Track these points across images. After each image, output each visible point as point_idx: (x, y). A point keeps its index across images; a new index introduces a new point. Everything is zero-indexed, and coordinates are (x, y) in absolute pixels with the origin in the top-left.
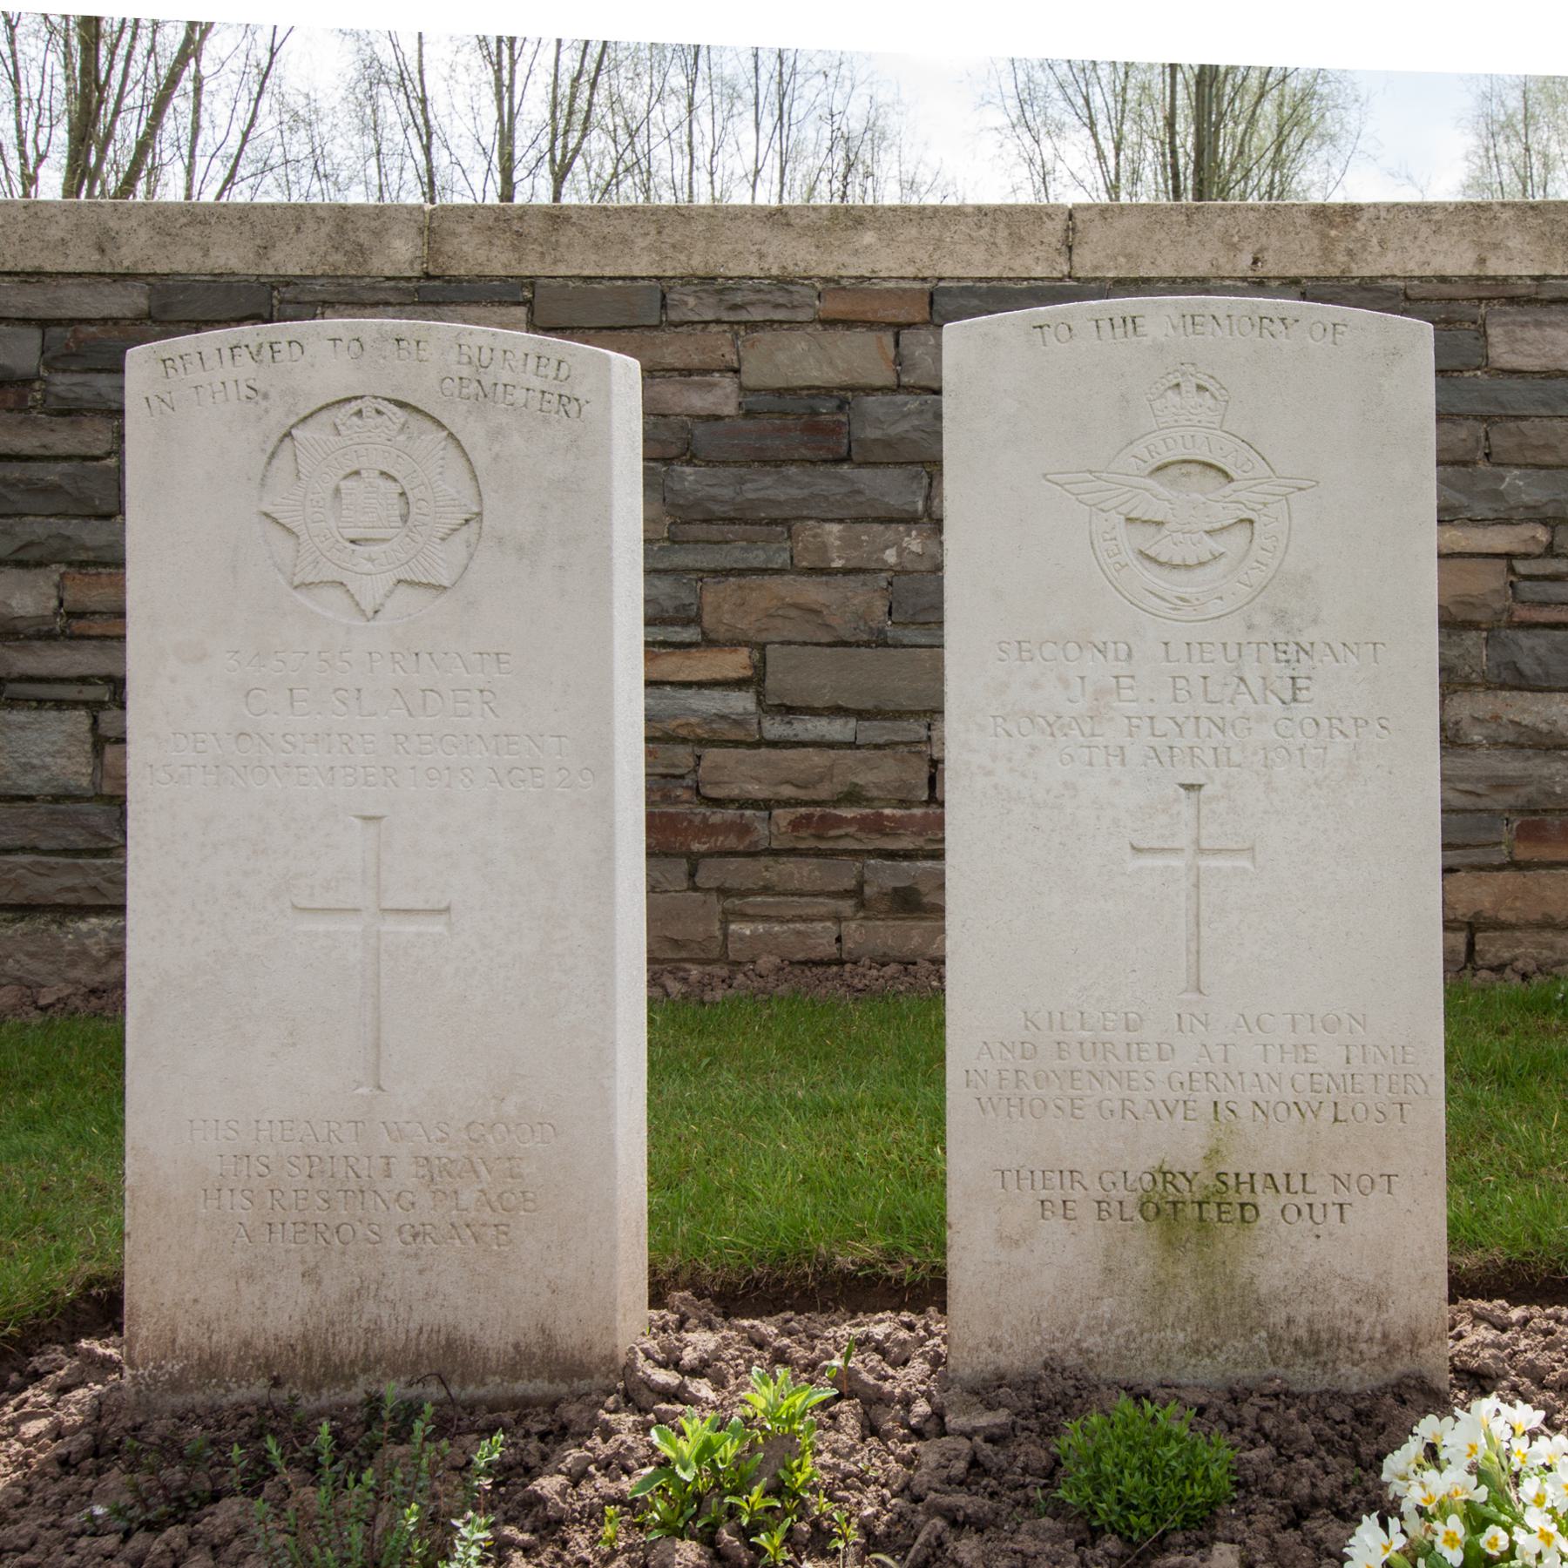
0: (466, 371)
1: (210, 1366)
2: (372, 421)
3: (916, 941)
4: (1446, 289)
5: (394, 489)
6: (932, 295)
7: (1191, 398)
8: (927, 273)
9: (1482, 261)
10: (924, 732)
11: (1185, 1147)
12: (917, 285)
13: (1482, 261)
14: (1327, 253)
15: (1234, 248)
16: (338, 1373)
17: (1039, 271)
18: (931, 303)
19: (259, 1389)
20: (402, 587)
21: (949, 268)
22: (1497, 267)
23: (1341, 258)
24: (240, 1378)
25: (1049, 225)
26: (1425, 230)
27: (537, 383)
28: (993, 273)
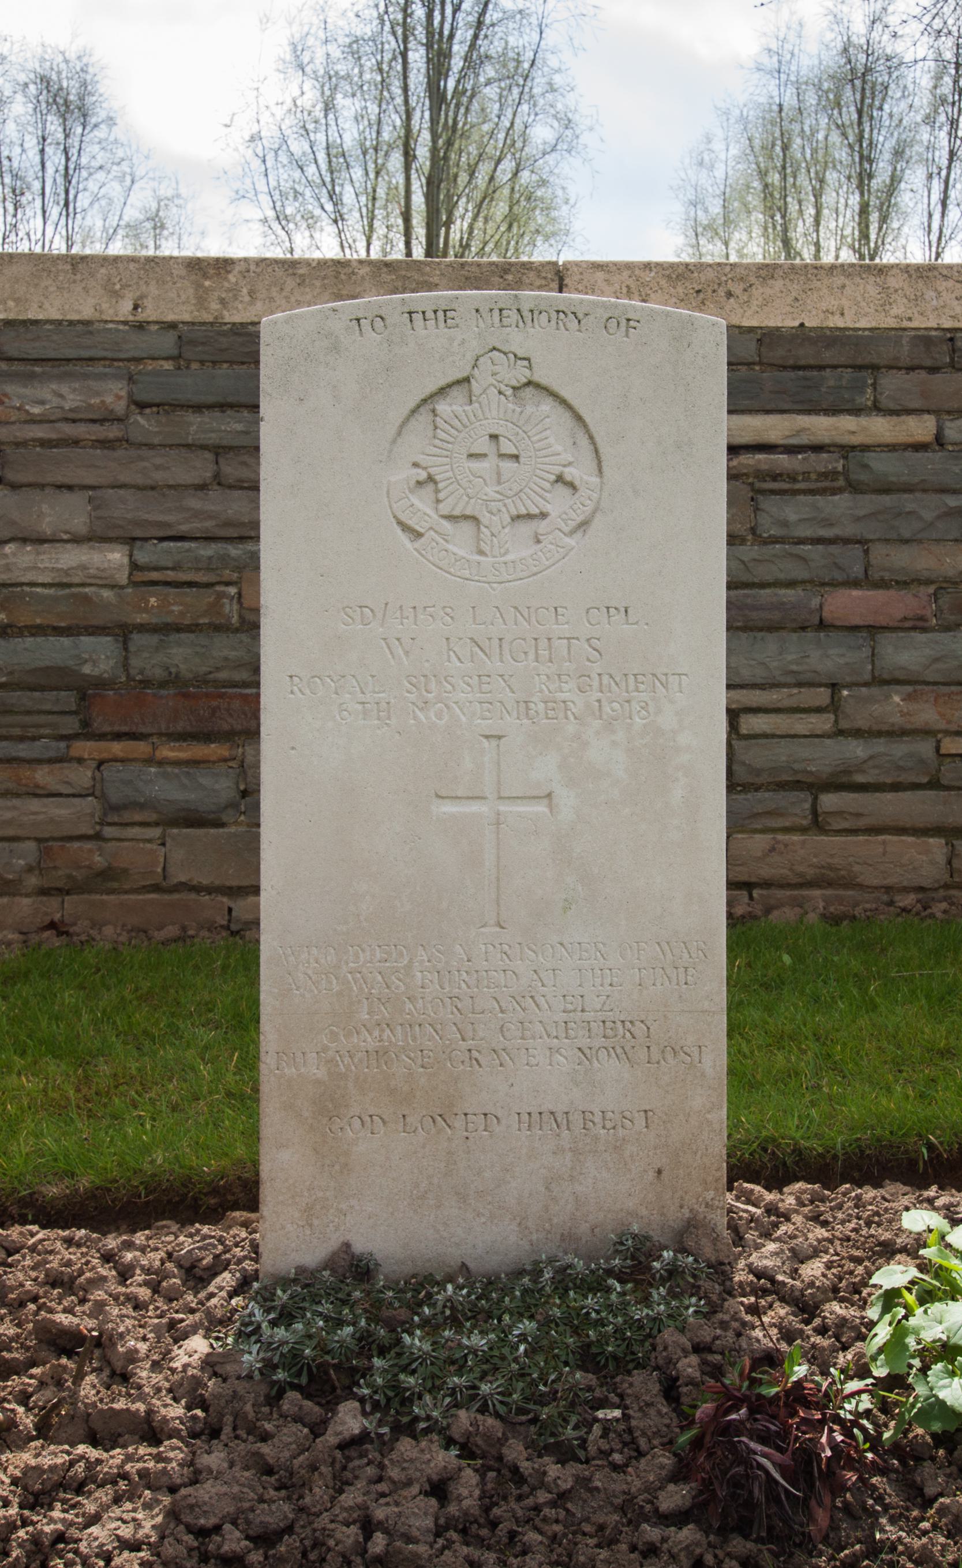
14: (201, 302)
23: (215, 306)
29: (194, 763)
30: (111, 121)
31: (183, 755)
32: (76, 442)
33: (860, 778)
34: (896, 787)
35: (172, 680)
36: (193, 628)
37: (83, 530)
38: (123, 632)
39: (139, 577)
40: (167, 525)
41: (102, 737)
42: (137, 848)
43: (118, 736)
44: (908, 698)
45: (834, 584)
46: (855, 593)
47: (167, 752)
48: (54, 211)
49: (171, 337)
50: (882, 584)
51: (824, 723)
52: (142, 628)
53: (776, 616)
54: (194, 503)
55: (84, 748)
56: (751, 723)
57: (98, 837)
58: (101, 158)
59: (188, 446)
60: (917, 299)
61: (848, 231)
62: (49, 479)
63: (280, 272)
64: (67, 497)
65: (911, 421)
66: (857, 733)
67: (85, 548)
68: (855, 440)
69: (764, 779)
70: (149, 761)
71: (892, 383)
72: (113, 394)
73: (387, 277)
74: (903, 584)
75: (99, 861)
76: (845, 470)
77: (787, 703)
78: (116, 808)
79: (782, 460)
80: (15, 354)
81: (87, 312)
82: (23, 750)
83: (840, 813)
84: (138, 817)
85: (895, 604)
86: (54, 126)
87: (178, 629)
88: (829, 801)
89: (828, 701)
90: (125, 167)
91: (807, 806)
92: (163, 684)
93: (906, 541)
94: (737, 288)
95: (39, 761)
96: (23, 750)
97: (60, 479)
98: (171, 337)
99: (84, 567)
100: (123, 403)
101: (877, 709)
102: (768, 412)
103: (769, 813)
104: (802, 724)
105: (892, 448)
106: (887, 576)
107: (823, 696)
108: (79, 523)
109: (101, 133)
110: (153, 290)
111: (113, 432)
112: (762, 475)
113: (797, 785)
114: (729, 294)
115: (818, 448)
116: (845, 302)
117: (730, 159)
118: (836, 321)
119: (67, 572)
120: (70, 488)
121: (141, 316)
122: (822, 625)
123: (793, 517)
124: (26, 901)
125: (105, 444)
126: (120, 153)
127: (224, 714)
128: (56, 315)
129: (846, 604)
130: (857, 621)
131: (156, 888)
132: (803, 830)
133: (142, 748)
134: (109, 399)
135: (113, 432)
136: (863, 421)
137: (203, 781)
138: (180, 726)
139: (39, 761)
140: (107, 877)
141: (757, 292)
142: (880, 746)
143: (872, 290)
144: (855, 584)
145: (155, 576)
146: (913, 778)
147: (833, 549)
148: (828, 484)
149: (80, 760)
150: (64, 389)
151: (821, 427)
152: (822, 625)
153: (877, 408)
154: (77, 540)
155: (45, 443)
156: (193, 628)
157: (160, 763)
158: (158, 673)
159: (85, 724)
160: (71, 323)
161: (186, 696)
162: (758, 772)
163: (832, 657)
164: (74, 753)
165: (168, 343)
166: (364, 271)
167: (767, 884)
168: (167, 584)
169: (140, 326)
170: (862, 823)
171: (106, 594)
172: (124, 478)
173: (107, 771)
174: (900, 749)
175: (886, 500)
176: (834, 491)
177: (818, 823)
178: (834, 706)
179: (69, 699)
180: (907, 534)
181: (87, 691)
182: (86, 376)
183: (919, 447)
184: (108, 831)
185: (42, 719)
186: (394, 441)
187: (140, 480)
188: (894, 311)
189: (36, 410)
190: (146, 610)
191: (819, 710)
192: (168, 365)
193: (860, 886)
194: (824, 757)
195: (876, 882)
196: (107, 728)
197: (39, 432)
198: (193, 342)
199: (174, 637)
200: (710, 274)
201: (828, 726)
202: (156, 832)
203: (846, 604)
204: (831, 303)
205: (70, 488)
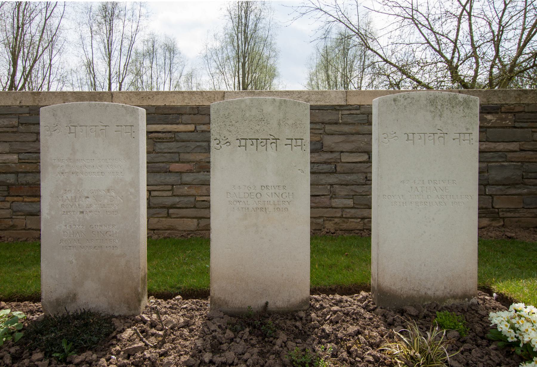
14: (34, 101)
23: (37, 102)
29: (31, 202)
30: (180, 53)
31: (30, 200)
32: (8, 132)
33: (178, 206)
34: (187, 208)
35: (27, 184)
36: (32, 172)
37: (8, 151)
38: (17, 173)
39: (20, 161)
40: (26, 150)
41: (13, 196)
42: (20, 221)
43: (17, 196)
44: (188, 188)
45: (172, 162)
46: (177, 164)
47: (26, 199)
48: (167, 72)
49: (28, 109)
50: (183, 162)
51: (170, 193)
52: (21, 172)
53: (159, 169)
54: (32, 145)
55: (8, 199)
56: (153, 194)
57: (11, 218)
58: (178, 61)
59: (32, 133)
60: (191, 99)
61: (324, 78)
63: (51, 94)
64: (5, 144)
65: (189, 126)
66: (178, 196)
67: (9, 155)
68: (176, 130)
69: (157, 206)
70: (23, 201)
71: (185, 118)
72: (15, 121)
73: (74, 95)
74: (188, 162)
75: (11, 223)
76: (174, 137)
77: (161, 189)
78: (14, 212)
79: (160, 135)
81: (10, 104)
83: (173, 214)
84: (19, 214)
85: (185, 167)
86: (168, 55)
87: (29, 173)
88: (171, 211)
90: (183, 63)
91: (166, 212)
92: (26, 185)
93: (189, 153)
94: (151, 97)
97: (4, 140)
98: (28, 109)
99: (8, 159)
100: (17, 123)
101: (181, 190)
103: (158, 214)
104: (165, 194)
105: (185, 132)
106: (184, 160)
107: (170, 187)
108: (7, 150)
109: (178, 56)
110: (24, 99)
111: (15, 130)
112: (157, 138)
113: (164, 207)
114: (149, 98)
115: (170, 132)
116: (175, 100)
117: (317, 60)
118: (173, 104)
119: (4, 160)
120: (6, 142)
121: (21, 104)
122: (170, 172)
123: (163, 147)
125: (13, 132)
126: (182, 60)
127: (34, 191)
128: (3, 104)
129: (175, 167)
130: (177, 171)
131: (24, 229)
132: (166, 217)
133: (21, 199)
134: (14, 122)
135: (15, 130)
136: (178, 126)
137: (34, 206)
138: (29, 194)
140: (13, 227)
141: (156, 97)
142: (182, 199)
143: (181, 97)
144: (177, 162)
145: (23, 161)
146: (189, 206)
147: (172, 155)
148: (171, 140)
149: (8, 201)
150: (5, 120)
151: (169, 127)
152: (170, 172)
153: (182, 123)
154: (7, 153)
156: (32, 172)
157: (26, 202)
158: (24, 182)
159: (9, 193)
161: (30, 187)
162: (155, 204)
163: (171, 179)
164: (6, 200)
165: (27, 110)
166: (69, 94)
167: (158, 229)
168: (27, 163)
169: (21, 107)
170: (178, 216)
171: (13, 165)
172: (18, 140)
173: (14, 204)
174: (186, 199)
175: (183, 144)
176: (172, 142)
177: (169, 216)
178: (172, 190)
179: (5, 188)
180: (189, 151)
181: (9, 186)
183: (191, 132)
184: (14, 217)
187: (21, 140)
188: (186, 101)
190: (22, 168)
191: (169, 191)
192: (28, 115)
193: (178, 230)
194: (169, 201)
195: (181, 229)
196: (13, 194)
199: (28, 174)
200: (145, 94)
201: (170, 194)
202: (24, 217)
203: (175, 167)
204: (172, 100)
205: (6, 142)
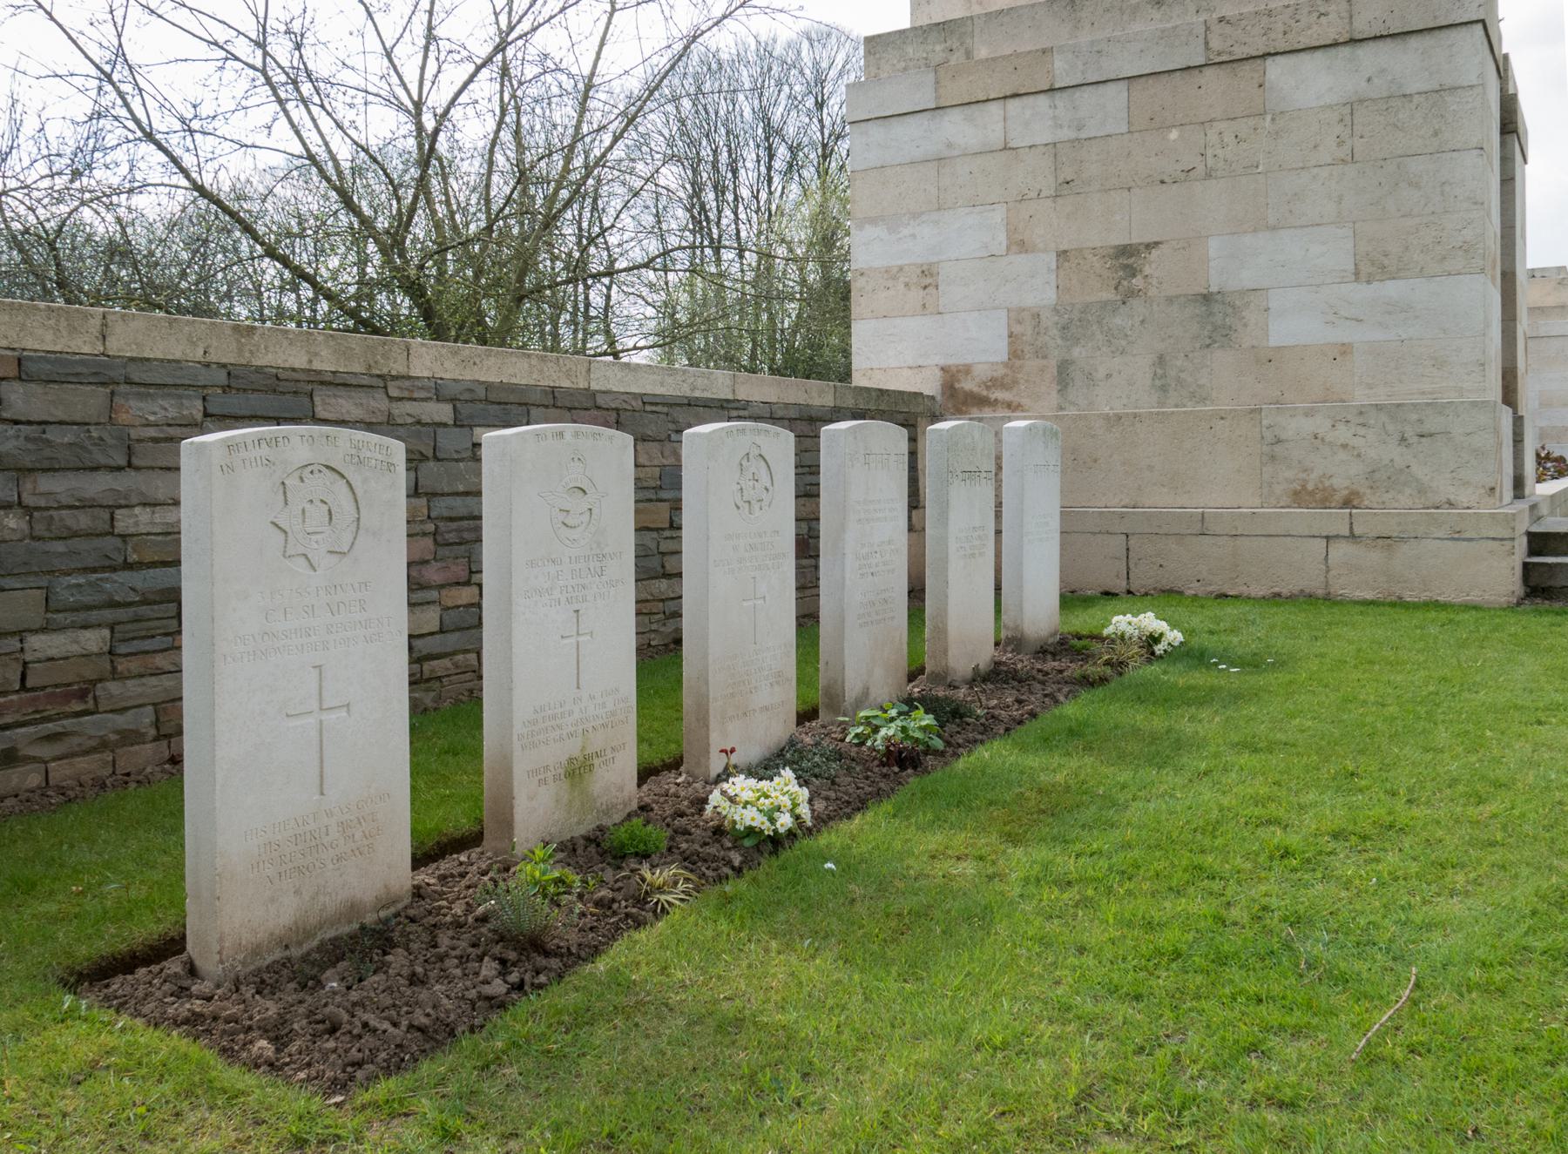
0: (353, 452)
1: (256, 951)
2: (317, 475)
3: (15, 781)
4: (295, 376)
5: (325, 508)
6: (19, 360)
7: (577, 463)
8: (16, 346)
9: (310, 361)
10: (19, 645)
11: (573, 748)
12: (9, 353)
13: (310, 361)
14: (240, 351)
15: (194, 344)
16: (308, 934)
17: (86, 349)
18: (19, 364)
19: (278, 954)
20: (303, 559)
21: (30, 343)
22: (317, 365)
23: (247, 354)
24: (270, 951)
25: (92, 321)
26: (285, 343)
27: (380, 457)
28: (58, 348)
62: (159, 464)
80: (137, 380)
81: (178, 356)
82: (147, 645)
89: (891, 437)
95: (155, 652)
96: (147, 645)
97: (165, 464)
102: (278, 421)
124: (148, 746)
139: (155, 652)
150: (165, 403)
155: (156, 440)
160: (169, 361)
169: (207, 365)
182: (180, 397)
185: (157, 623)
186: (1431, 435)
189: (152, 418)
197: (152, 432)
198: (237, 377)
